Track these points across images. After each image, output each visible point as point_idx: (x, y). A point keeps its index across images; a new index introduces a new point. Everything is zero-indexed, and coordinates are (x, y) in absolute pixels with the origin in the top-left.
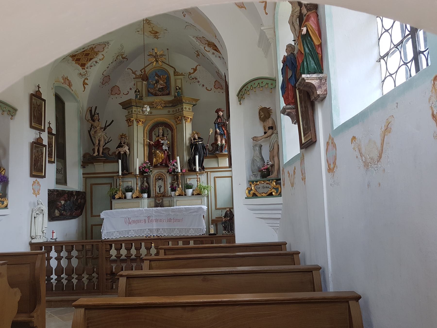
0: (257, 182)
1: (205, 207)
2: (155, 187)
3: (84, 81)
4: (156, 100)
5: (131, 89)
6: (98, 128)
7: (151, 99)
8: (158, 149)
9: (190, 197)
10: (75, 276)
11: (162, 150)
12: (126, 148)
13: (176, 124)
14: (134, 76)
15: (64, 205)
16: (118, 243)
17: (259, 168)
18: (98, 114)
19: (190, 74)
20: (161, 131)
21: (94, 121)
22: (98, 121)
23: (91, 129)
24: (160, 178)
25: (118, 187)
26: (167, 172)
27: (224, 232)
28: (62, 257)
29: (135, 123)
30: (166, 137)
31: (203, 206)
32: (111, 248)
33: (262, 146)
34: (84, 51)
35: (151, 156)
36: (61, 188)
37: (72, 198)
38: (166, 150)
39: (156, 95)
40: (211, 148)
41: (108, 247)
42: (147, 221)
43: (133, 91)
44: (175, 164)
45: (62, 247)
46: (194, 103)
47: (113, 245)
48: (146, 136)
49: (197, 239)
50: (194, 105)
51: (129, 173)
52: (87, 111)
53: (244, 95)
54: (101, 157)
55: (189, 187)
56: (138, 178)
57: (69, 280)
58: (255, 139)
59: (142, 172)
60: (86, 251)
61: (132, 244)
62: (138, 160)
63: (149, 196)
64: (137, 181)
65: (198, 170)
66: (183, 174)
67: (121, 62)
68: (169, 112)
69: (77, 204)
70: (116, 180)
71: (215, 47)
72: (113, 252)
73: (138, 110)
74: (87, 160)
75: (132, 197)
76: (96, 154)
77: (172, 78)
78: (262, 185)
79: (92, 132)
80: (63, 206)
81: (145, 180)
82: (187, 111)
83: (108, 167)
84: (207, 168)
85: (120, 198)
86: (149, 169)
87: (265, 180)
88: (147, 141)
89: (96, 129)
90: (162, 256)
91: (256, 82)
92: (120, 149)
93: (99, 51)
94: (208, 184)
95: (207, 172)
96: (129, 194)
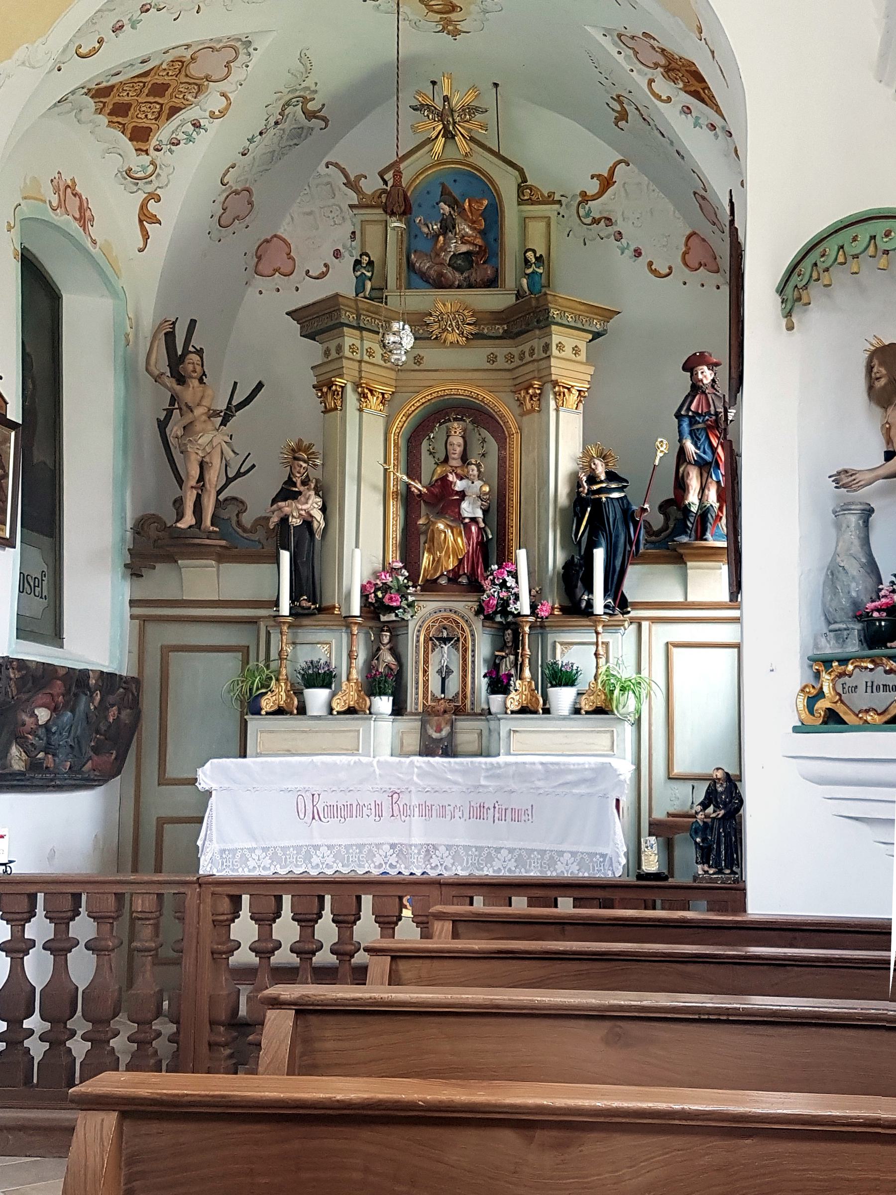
0: (844, 661)
1: (625, 768)
2: (425, 671)
3: (143, 207)
4: (440, 306)
5: (337, 254)
6: (199, 411)
7: (421, 299)
8: (441, 514)
9: (564, 718)
10: (79, 1024)
11: (460, 518)
12: (312, 505)
13: (518, 411)
14: (354, 198)
15: (46, 726)
16: (267, 894)
17: (855, 604)
18: (200, 352)
19: (585, 198)
20: (457, 440)
21: (181, 380)
22: (201, 381)
23: (169, 413)
24: (445, 636)
25: (273, 665)
26: (477, 613)
27: (700, 869)
28: (33, 943)
29: (351, 398)
30: (478, 466)
31: (615, 762)
32: (235, 915)
33: (871, 511)
34: (146, 74)
35: (411, 543)
36: (36, 653)
37: (84, 699)
38: (474, 520)
39: (440, 283)
40: (657, 521)
41: (225, 905)
42: (386, 813)
43: (348, 262)
44: (510, 582)
45: (33, 898)
46: (598, 324)
47: (246, 899)
48: (397, 459)
49: (585, 890)
50: (597, 335)
51: (321, 610)
52: (154, 337)
53: (805, 287)
54: (209, 535)
55: (563, 677)
56: (355, 630)
57: (56, 1040)
58: (844, 479)
59: (375, 608)
60: (133, 920)
61: (321, 899)
62: (362, 553)
63: (398, 710)
64: (351, 644)
65: (599, 607)
66: (541, 627)
67: (300, 133)
68: (492, 359)
69: (103, 728)
70: (268, 634)
71: (693, 81)
72: (244, 929)
73: (367, 344)
74: (152, 545)
75: (331, 710)
76: (189, 520)
77: (511, 213)
78: (867, 677)
79: (174, 430)
80: (41, 732)
81: (386, 640)
82: (568, 356)
83: (238, 581)
84: (638, 605)
85: (280, 711)
86: (404, 597)
87: (880, 657)
88: (396, 479)
89: (189, 417)
90: (442, 938)
91: (863, 232)
92: (286, 507)
93: (208, 78)
94: (639, 671)
95: (638, 622)
96: (317, 698)
